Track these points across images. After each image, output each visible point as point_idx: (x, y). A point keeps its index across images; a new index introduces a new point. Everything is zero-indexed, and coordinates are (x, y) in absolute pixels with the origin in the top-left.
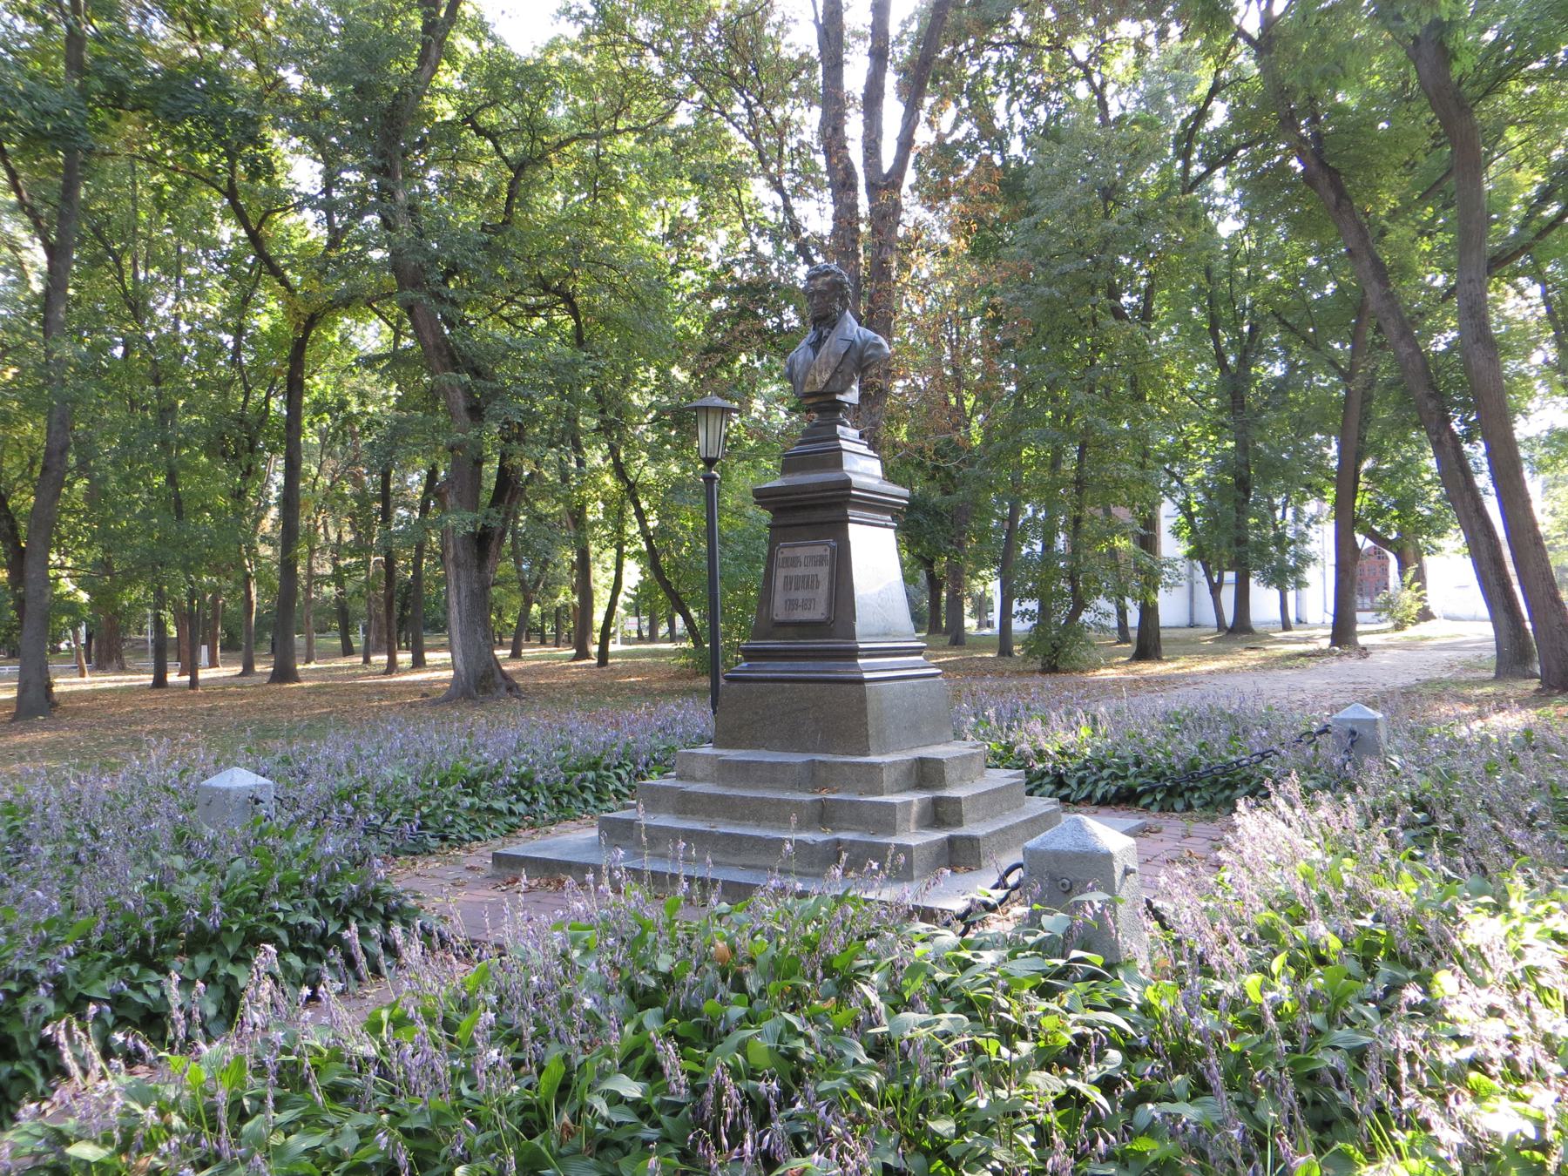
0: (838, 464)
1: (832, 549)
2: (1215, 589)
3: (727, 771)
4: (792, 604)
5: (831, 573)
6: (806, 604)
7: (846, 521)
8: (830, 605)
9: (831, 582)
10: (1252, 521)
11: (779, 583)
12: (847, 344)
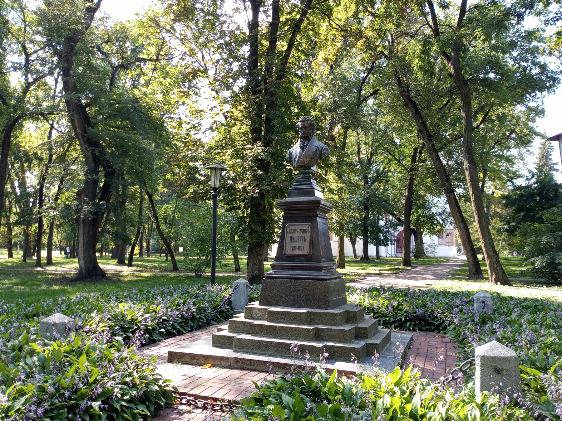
0: (312, 194)
2: (354, 243)
3: (272, 316)
4: (294, 248)
5: (311, 236)
7: (316, 216)
8: (310, 248)
10: (164, 248)
11: (288, 239)
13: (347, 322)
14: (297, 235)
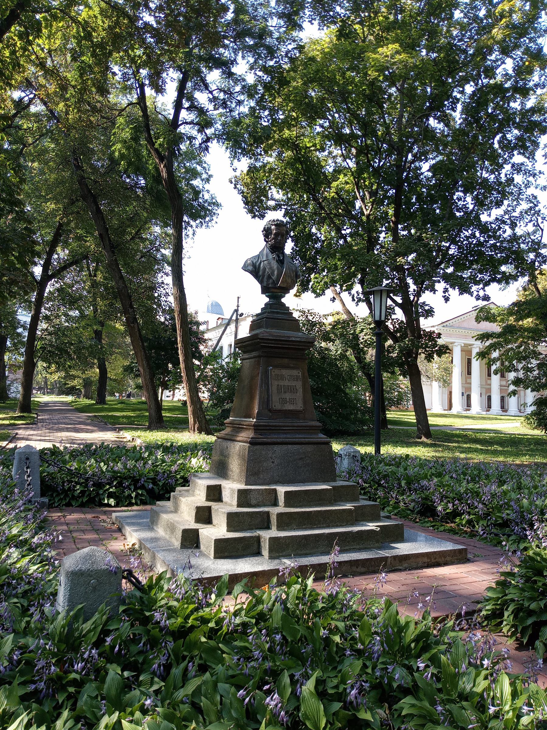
4: (284, 401)
14: (286, 383)
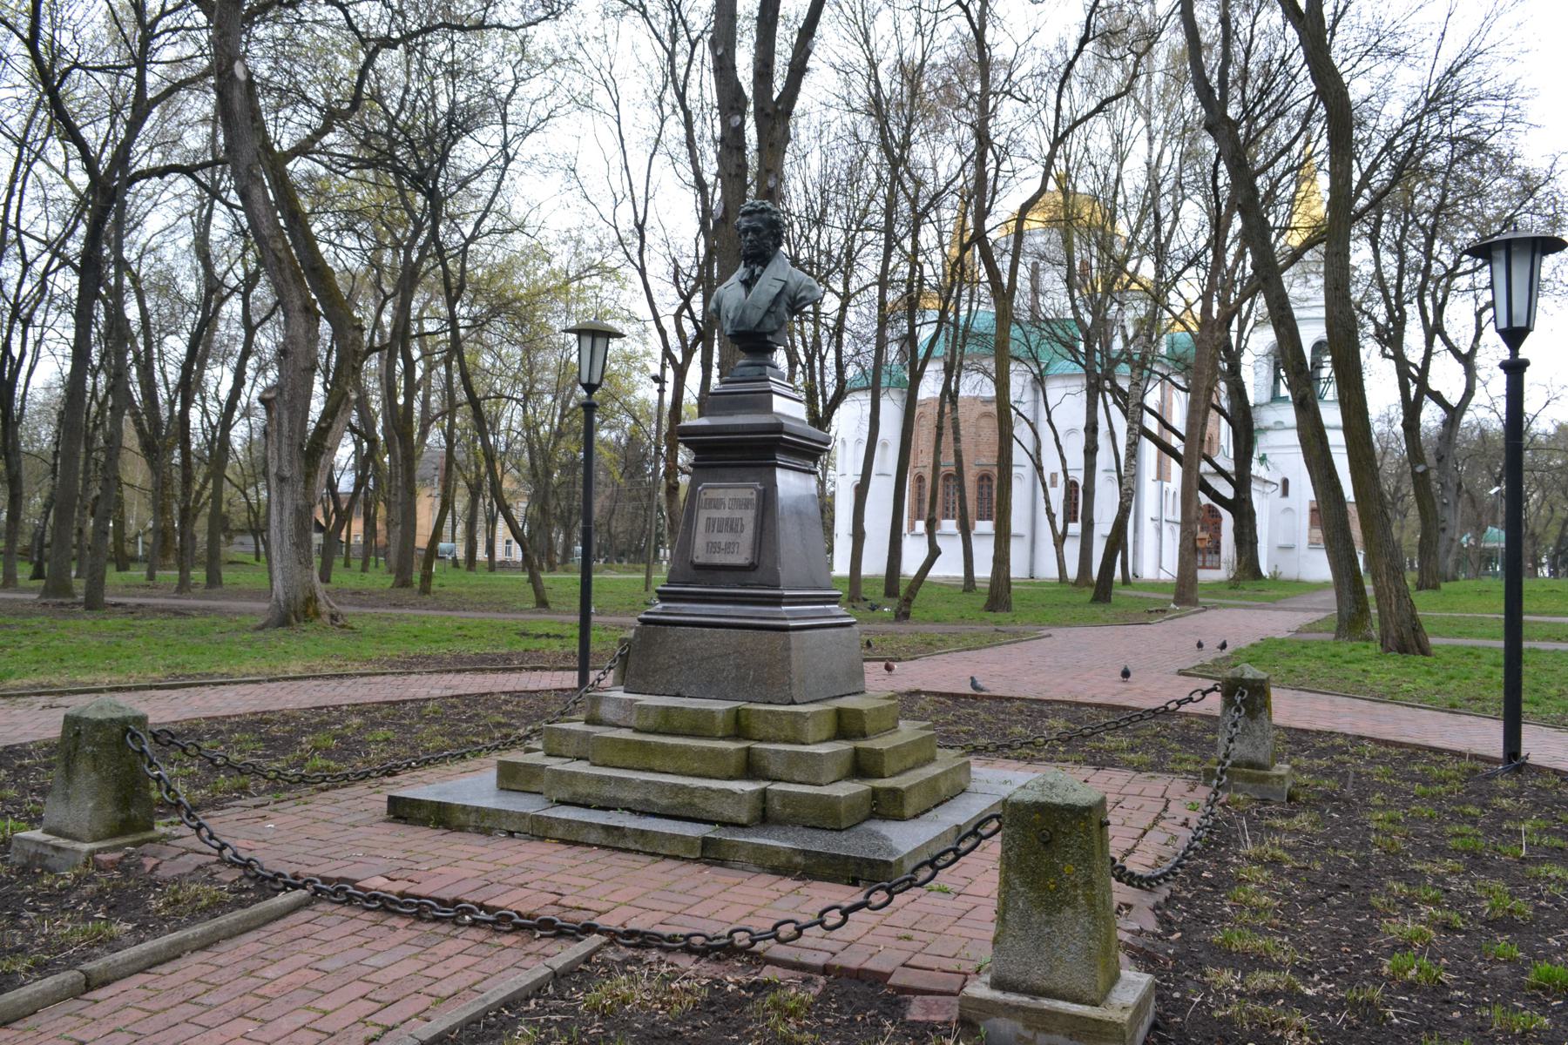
1: (758, 492)
4: (713, 547)
6: (730, 548)
9: (756, 527)
12: (780, 285)
13: (841, 733)
14: (724, 513)
